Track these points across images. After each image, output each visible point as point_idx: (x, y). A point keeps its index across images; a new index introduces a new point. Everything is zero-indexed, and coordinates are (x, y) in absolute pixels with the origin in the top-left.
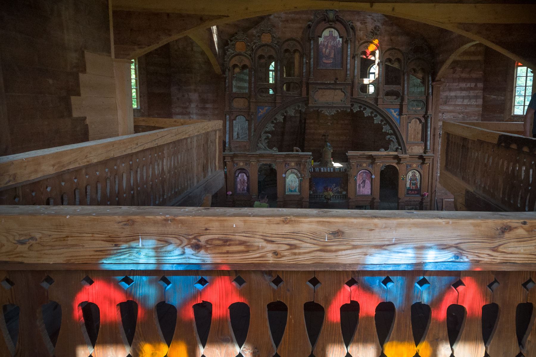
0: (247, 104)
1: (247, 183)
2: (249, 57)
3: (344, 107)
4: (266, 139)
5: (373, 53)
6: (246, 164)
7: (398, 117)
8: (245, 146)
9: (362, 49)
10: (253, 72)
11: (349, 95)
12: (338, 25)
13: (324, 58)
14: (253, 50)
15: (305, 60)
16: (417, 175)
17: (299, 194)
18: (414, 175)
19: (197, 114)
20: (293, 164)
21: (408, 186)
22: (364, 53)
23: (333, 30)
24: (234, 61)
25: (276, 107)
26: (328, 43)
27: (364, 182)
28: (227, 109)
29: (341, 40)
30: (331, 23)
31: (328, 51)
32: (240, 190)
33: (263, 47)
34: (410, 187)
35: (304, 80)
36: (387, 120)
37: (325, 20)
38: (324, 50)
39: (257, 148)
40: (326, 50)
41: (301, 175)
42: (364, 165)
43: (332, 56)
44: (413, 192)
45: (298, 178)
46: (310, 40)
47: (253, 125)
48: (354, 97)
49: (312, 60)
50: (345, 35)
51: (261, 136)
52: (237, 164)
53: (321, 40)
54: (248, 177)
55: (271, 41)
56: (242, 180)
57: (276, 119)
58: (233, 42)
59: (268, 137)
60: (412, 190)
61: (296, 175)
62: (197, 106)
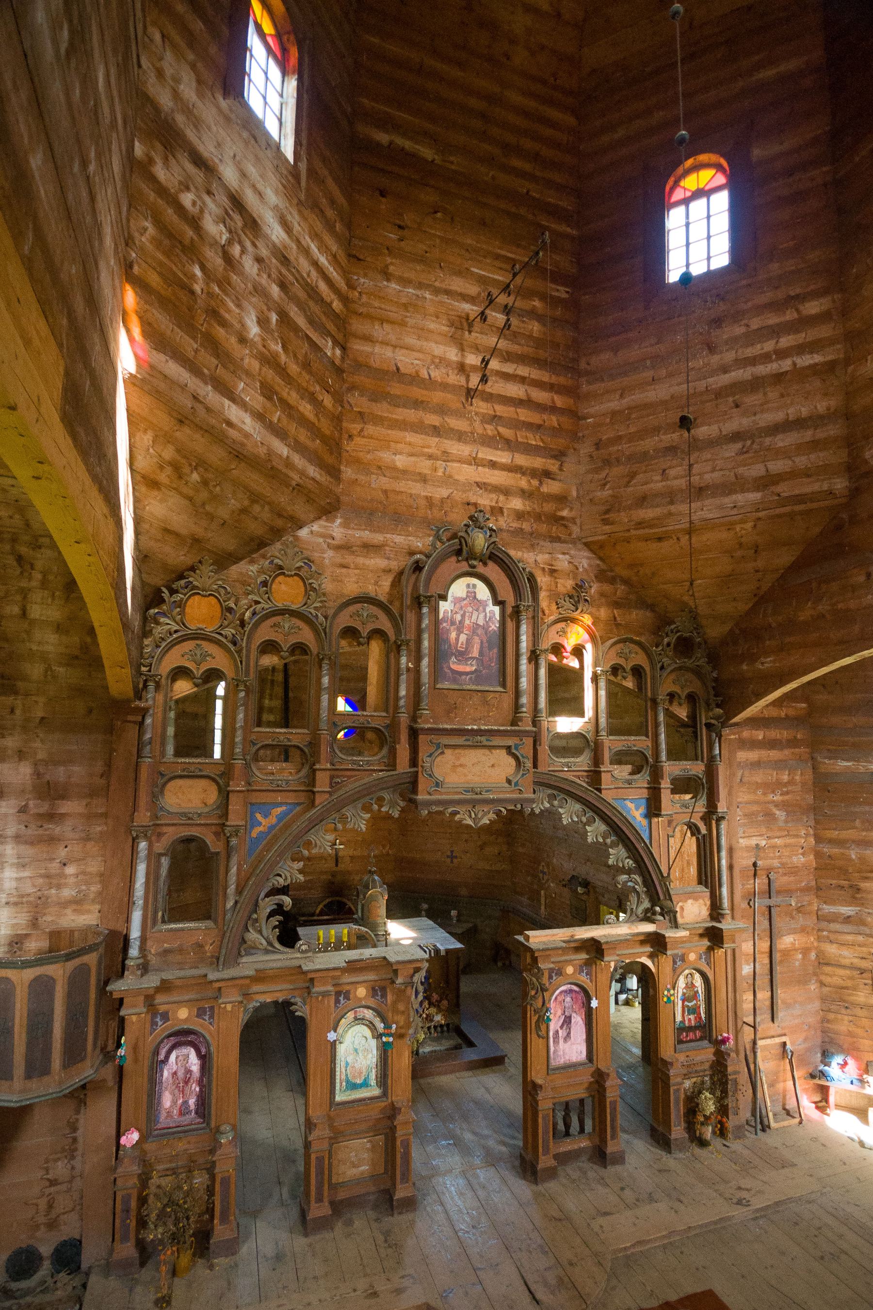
0: (213, 796)
1: (200, 1083)
2: (230, 645)
3: (514, 801)
4: (271, 914)
5: (578, 651)
6: (201, 1013)
7: (645, 822)
8: (201, 946)
10: (242, 694)
11: (529, 764)
12: (493, 571)
13: (453, 659)
14: (243, 624)
15: (403, 660)
16: (698, 981)
17: (376, 1092)
18: (690, 986)
19: (18, 838)
20: (361, 992)
21: (679, 1018)
22: (557, 649)
23: (475, 581)
24: (174, 659)
25: (312, 804)
26: (463, 616)
27: (568, 1021)
28: (143, 817)
29: (497, 609)
30: (475, 563)
31: (463, 638)
32: (169, 1113)
33: (278, 619)
34: (683, 1022)
35: (404, 718)
36: (620, 831)
37: (459, 552)
38: (453, 635)
39: (242, 947)
41: (388, 1027)
42: (570, 970)
43: (475, 653)
44: (691, 1035)
45: (378, 1036)
46: (420, 605)
47: (234, 870)
48: (539, 770)
49: (425, 662)
50: (511, 600)
51: (256, 904)
52: (165, 1017)
53: (444, 607)
54: (204, 1059)
55: (301, 600)
56: (181, 1074)
57: (308, 844)
58: (178, 597)
59: (280, 906)
60: (690, 1029)
61: (372, 1026)
62: (23, 810)
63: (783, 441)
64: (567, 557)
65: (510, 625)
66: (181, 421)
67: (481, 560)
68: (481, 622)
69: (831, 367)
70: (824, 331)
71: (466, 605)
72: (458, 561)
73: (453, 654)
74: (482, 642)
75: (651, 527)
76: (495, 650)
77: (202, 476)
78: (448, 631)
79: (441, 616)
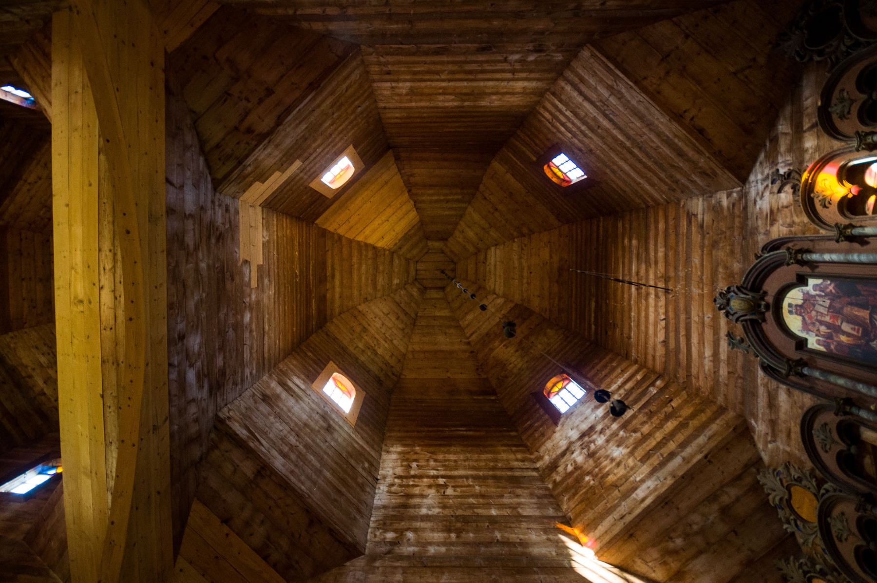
9: (832, 215)
12: (771, 286)
26: (822, 323)
29: (812, 282)
31: (846, 327)
38: (843, 338)
40: (844, 333)
43: (864, 314)
53: (813, 343)
63: (594, 97)
64: (758, 199)
65: (822, 269)
66: (631, 536)
67: (762, 299)
68: (828, 303)
69: (554, 94)
70: (549, 106)
71: (810, 318)
72: (764, 320)
73: (867, 343)
74: (851, 304)
75: (694, 145)
76: (859, 287)
77: (679, 536)
78: (840, 344)
79: (822, 348)
